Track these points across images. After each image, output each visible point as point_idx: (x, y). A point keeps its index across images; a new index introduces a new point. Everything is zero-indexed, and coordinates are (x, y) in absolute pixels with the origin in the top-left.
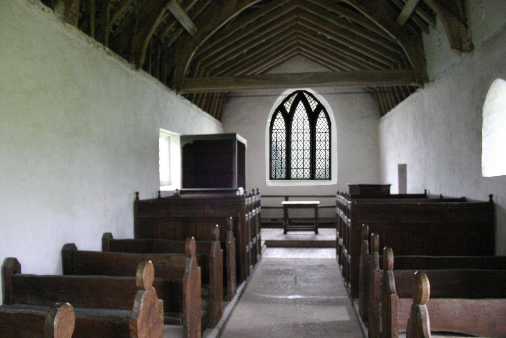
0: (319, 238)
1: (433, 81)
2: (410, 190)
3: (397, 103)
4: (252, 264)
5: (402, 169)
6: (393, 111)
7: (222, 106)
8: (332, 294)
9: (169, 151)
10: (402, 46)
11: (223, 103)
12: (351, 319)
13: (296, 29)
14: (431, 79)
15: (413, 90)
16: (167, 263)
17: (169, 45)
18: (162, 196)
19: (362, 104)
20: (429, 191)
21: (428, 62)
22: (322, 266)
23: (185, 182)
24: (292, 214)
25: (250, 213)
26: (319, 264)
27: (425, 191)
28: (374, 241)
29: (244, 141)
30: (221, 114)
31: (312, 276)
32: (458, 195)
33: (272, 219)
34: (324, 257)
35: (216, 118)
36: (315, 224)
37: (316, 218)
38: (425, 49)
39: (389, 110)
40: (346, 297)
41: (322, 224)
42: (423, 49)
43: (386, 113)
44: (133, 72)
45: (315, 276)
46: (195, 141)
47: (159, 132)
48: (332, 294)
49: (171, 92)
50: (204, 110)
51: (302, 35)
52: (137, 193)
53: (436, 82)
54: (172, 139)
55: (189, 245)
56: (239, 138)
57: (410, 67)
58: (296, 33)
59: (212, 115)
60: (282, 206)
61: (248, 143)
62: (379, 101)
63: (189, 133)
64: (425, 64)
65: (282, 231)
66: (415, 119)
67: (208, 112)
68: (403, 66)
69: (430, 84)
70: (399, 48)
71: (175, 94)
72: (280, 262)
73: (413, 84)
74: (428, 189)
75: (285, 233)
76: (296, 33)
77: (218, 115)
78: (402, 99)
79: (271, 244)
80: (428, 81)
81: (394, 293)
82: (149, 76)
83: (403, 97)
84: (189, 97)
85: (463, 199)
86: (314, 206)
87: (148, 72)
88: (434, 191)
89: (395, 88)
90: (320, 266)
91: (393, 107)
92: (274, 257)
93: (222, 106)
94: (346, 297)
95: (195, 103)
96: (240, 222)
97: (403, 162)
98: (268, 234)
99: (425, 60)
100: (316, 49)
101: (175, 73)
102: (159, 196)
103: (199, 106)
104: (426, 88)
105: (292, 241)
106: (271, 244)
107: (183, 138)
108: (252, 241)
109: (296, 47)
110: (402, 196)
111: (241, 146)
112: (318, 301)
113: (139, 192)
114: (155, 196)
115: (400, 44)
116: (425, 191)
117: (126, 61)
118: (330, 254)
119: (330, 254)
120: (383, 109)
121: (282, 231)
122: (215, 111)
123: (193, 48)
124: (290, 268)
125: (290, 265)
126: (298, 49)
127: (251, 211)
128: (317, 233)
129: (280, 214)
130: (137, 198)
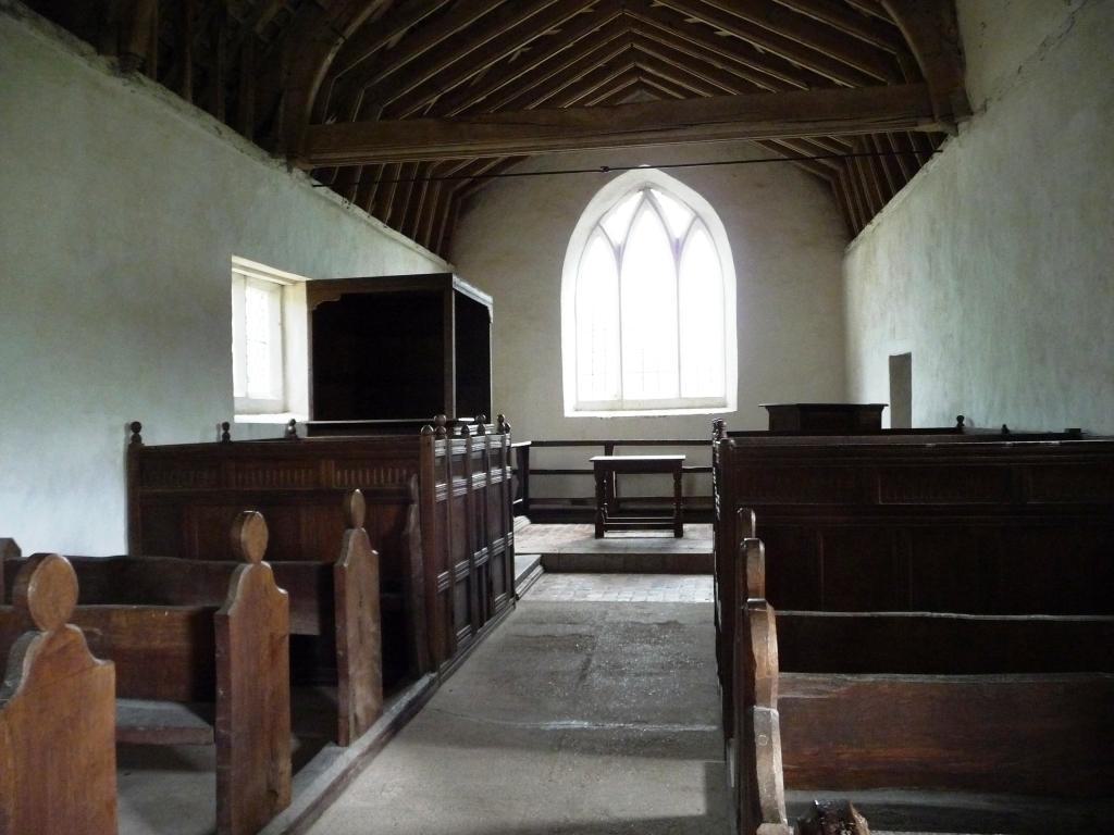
0: (683, 547)
1: (985, 108)
2: (917, 422)
3: (888, 197)
4: (469, 621)
5: (900, 367)
6: (877, 219)
7: (450, 222)
8: (675, 715)
9: (283, 325)
10: (902, 29)
11: (451, 214)
12: (710, 813)
13: (624, 7)
14: (976, 103)
15: (928, 147)
16: (100, 634)
17: (259, 28)
18: (234, 437)
19: (799, 204)
20: (971, 422)
21: (971, 57)
22: (670, 626)
23: (319, 404)
24: (628, 487)
25: (459, 481)
26: (664, 620)
27: (960, 419)
28: (745, 567)
29: (485, 298)
30: (448, 239)
31: (635, 655)
32: (1060, 427)
33: (575, 501)
34: (687, 600)
35: (432, 249)
36: (674, 515)
37: (678, 498)
38: (962, 18)
39: (869, 219)
40: (714, 728)
41: (698, 512)
42: (955, 22)
43: (861, 228)
44: (116, 83)
45: (647, 654)
46: (344, 296)
47: (230, 265)
48: (675, 715)
49: (274, 163)
50: (392, 224)
51: (642, 26)
52: (136, 427)
53: (992, 107)
54: (290, 291)
55: (27, 583)
56: (462, 285)
57: (919, 78)
58: (623, 20)
59: (419, 240)
60: (591, 467)
61: (494, 304)
62: (845, 209)
63: (338, 272)
64: (963, 65)
65: (590, 529)
66: (932, 231)
67: (407, 232)
68: (900, 79)
69: (976, 119)
70: (892, 34)
71: (284, 169)
72: (565, 616)
73: (927, 127)
74: (966, 415)
75: (599, 535)
76: (623, 20)
77: (440, 243)
78: (901, 184)
79: (554, 564)
80: (968, 112)
81: (777, 820)
82: (188, 106)
83: (903, 178)
84: (322, 176)
85: (1074, 433)
86: (672, 467)
87: (182, 95)
88: (984, 417)
89: (874, 138)
90: (665, 625)
91: (879, 209)
92: (554, 598)
93: (450, 222)
94: (714, 728)
95: (362, 204)
96: (415, 507)
97: (899, 350)
98: (531, 539)
99: (960, 52)
100: (679, 66)
101: (281, 109)
102: (226, 436)
103: (377, 214)
104: (963, 134)
105: (612, 556)
106: (554, 564)
107: (314, 288)
108: (468, 555)
109: (630, 66)
110: (900, 431)
111: (474, 315)
112: (627, 740)
113: (142, 423)
114: (213, 437)
115: (897, 21)
116: (960, 419)
117: (86, 47)
118: (700, 591)
119: (700, 591)
120: (852, 218)
121: (590, 529)
122: (428, 234)
123: (330, 43)
124: (584, 630)
125: (583, 623)
126: (637, 71)
127: (467, 475)
128: (679, 534)
129: (585, 488)
130: (136, 439)
